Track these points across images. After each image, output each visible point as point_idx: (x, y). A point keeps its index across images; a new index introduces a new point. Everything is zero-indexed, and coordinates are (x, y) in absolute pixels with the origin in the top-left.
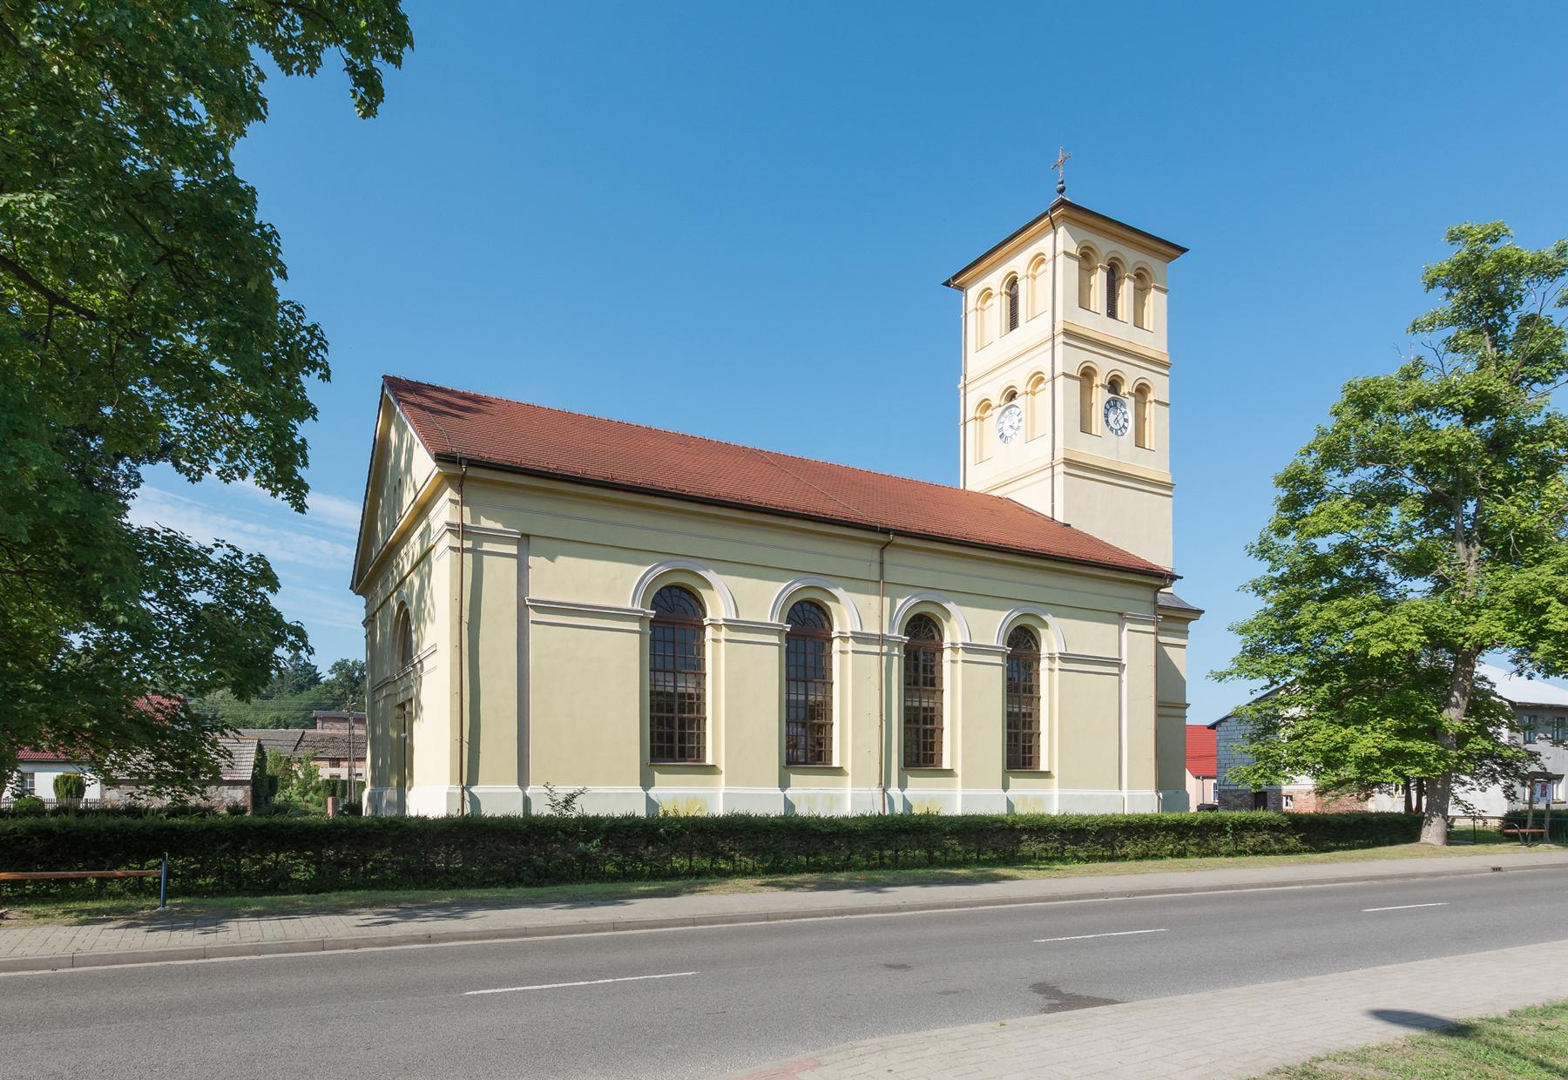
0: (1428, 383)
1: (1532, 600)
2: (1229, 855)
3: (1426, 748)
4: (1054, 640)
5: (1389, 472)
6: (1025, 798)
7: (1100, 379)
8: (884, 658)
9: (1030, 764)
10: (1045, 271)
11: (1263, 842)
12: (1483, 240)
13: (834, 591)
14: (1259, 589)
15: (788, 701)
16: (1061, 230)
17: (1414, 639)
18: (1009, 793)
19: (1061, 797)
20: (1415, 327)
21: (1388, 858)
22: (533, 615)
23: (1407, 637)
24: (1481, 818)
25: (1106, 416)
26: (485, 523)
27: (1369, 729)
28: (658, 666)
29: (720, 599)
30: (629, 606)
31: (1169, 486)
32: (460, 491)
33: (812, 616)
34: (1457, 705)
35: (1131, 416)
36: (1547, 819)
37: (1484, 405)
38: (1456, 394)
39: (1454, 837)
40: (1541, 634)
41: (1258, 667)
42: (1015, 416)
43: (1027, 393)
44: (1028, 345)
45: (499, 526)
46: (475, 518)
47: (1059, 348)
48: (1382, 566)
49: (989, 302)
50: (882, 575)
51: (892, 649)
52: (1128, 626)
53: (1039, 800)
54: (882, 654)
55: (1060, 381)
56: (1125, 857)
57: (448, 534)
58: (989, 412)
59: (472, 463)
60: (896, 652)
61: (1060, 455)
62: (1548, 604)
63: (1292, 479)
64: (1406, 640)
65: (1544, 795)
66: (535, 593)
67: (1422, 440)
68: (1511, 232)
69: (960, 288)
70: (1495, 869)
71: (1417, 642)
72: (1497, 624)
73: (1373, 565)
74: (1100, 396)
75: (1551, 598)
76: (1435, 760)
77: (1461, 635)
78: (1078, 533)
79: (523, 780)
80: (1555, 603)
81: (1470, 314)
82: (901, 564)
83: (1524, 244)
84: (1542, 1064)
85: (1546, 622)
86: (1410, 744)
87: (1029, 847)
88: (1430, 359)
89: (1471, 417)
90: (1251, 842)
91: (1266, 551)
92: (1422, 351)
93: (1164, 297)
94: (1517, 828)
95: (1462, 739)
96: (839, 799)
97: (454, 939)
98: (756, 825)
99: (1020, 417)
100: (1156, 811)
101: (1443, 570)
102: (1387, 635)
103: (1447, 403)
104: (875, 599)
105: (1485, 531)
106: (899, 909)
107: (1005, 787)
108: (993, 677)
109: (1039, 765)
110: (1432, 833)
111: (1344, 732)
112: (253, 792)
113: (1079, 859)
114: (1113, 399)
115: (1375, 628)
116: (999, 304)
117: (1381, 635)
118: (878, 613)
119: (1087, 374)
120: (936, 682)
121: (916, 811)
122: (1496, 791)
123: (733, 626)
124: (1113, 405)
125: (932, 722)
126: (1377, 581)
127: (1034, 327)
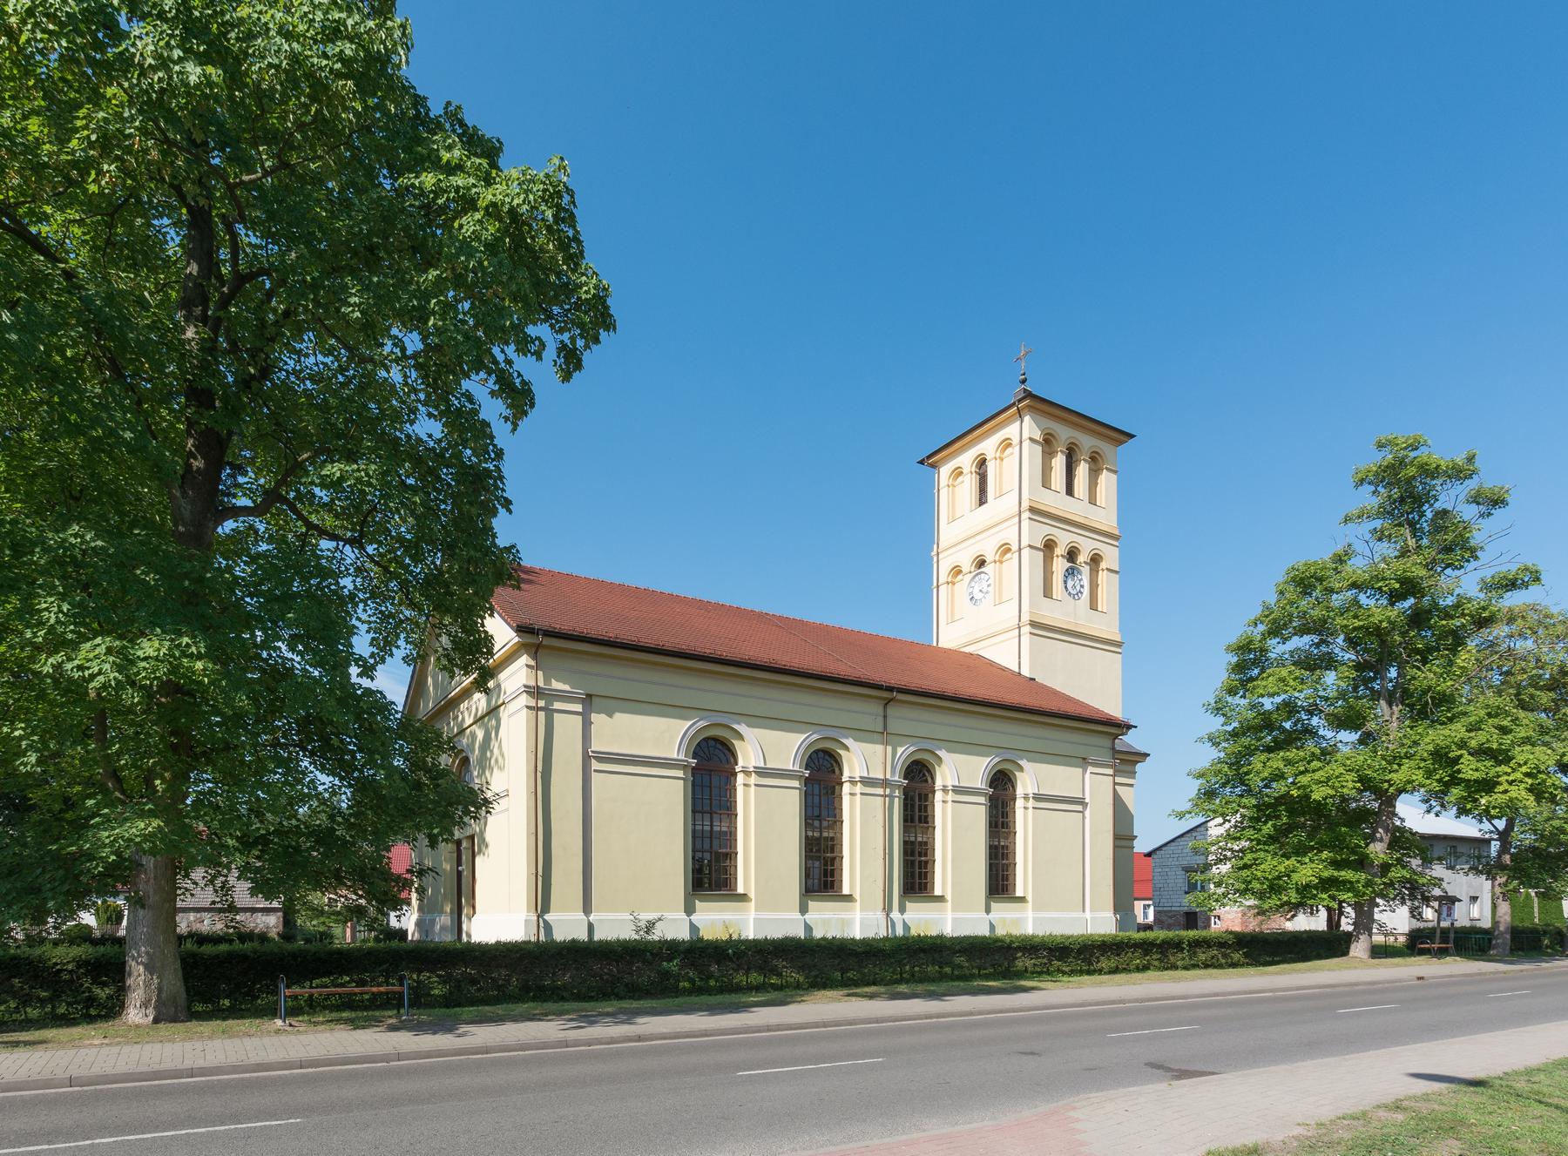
0: (1357, 567)
1: (1447, 753)
2: (1186, 968)
3: (1357, 876)
4: (1028, 782)
5: (1322, 642)
6: (1004, 920)
7: (1060, 550)
8: (887, 799)
9: (926, 889)
10: (1012, 454)
11: (1213, 958)
12: (1406, 448)
13: (845, 741)
14: (1214, 741)
15: (694, 831)
16: (1027, 419)
17: (1350, 786)
18: (991, 916)
19: (1035, 919)
20: (1347, 520)
21: (1329, 970)
22: (595, 765)
23: (1344, 784)
24: (1393, 934)
25: (1065, 582)
26: (557, 685)
27: (1307, 860)
28: (700, 808)
29: (750, 749)
30: (675, 756)
31: (1119, 644)
32: (535, 657)
34: (1381, 840)
35: (1086, 583)
36: (1452, 936)
37: (1409, 587)
38: (1384, 579)
39: (1379, 952)
40: (1454, 781)
41: (1212, 807)
43: (995, 562)
44: (996, 520)
45: (567, 688)
46: (547, 681)
47: (1025, 524)
48: (1315, 721)
49: (960, 479)
50: (885, 728)
51: (893, 791)
52: (1090, 769)
53: (1018, 921)
54: (886, 796)
55: (1026, 552)
56: (1100, 972)
57: (525, 694)
58: (960, 577)
60: (897, 794)
61: (1026, 618)
62: (1461, 756)
63: (1244, 647)
64: (1343, 787)
65: (1449, 915)
66: (596, 746)
67: (1356, 617)
68: (1429, 442)
69: (933, 466)
70: (1420, 978)
71: (1352, 789)
72: (1417, 772)
73: (1308, 719)
74: (1060, 565)
75: (1462, 752)
76: (1363, 886)
77: (1386, 781)
78: (1043, 687)
79: (587, 909)
80: (1466, 756)
81: (1393, 509)
82: (903, 718)
83: (1440, 452)
84: (1540, 1102)
85: (1459, 771)
86: (1343, 873)
87: (1023, 962)
88: (1359, 547)
89: (1395, 597)
90: (1202, 957)
91: (1221, 709)
92: (1352, 540)
93: (1114, 477)
94: (1418, 943)
95: (1385, 868)
96: (850, 923)
97: (657, 1039)
98: (804, 946)
100: (1114, 932)
101: (1371, 726)
102: (1325, 782)
103: (1376, 586)
104: (879, 748)
105: (1406, 693)
106: (971, 1014)
107: (988, 911)
108: (977, 815)
109: (1015, 891)
110: (1359, 949)
111: (1287, 863)
112: (284, 917)
113: (1064, 973)
114: (1071, 568)
115: (1317, 776)
116: (969, 483)
117: (1321, 782)
118: (882, 760)
119: (1049, 546)
120: (929, 819)
121: (914, 932)
122: (1403, 911)
123: (762, 772)
124: (1071, 572)
125: (926, 855)
126: (1310, 732)
127: (1003, 503)
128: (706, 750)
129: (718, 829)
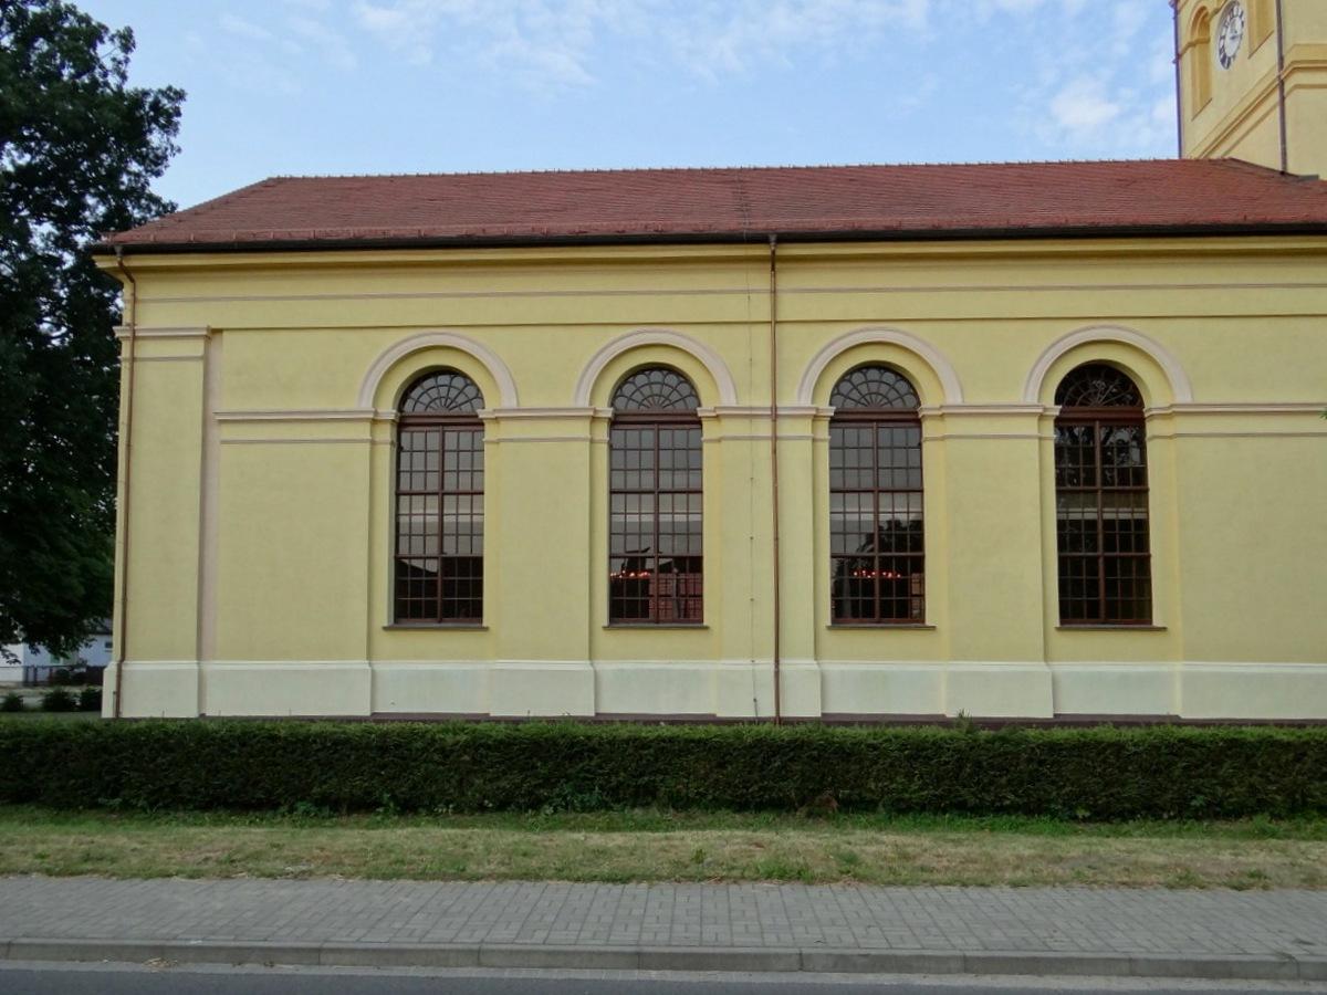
42: (1237, 18)
59: (786, 238)
129: (856, 517)
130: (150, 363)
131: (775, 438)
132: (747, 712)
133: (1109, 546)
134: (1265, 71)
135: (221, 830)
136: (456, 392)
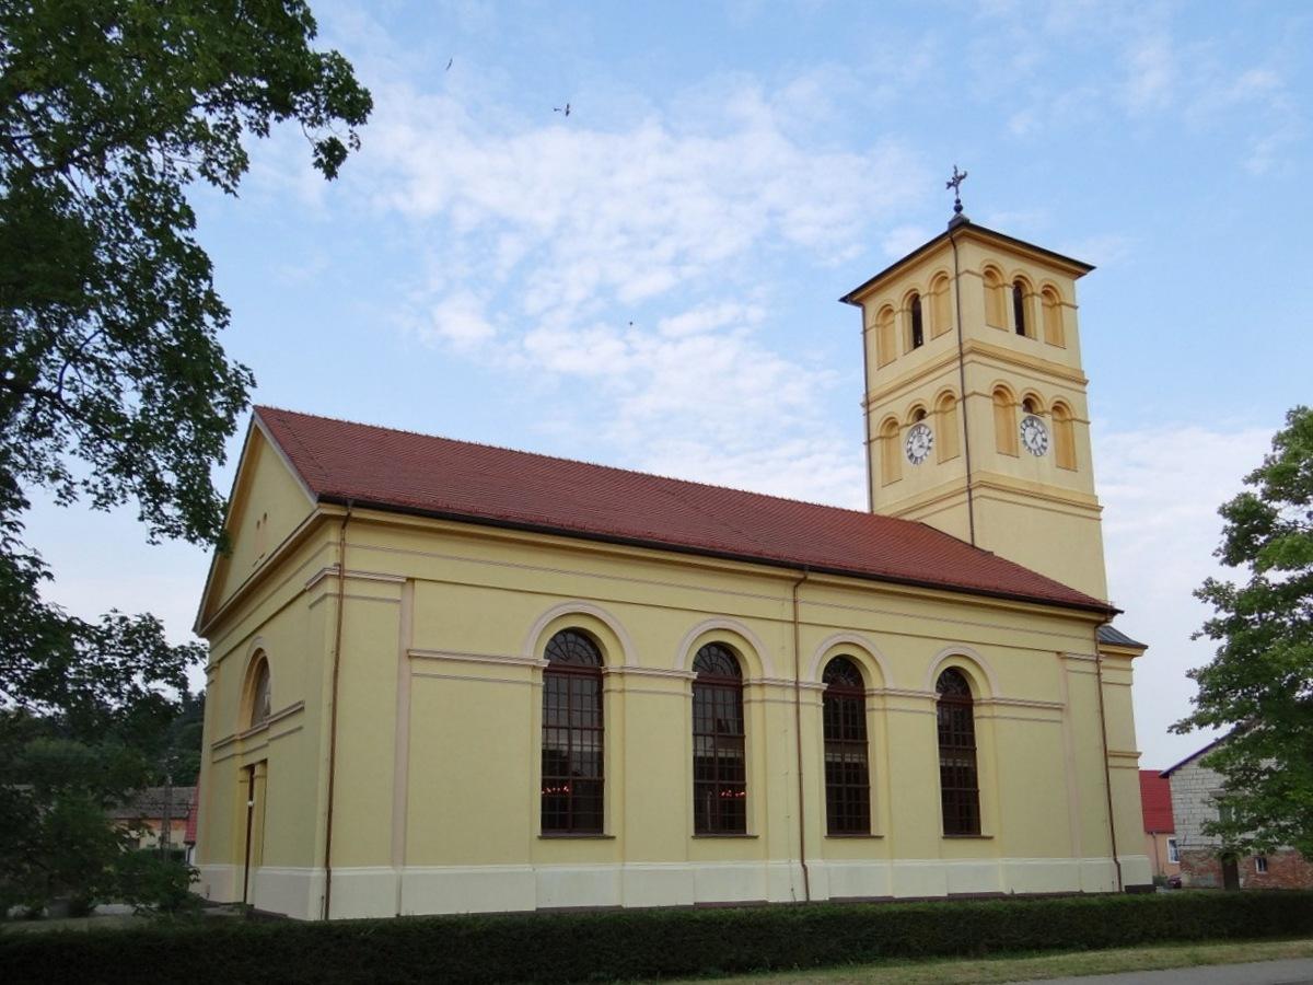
33: (578, 649)
49: (890, 318)
78: (1002, 561)
99: (930, 437)
128: (707, 659)
129: (579, 749)
130: (358, 602)
131: (797, 703)
132: (787, 899)
133: (848, 781)
134: (952, 478)
135: (1258, 949)
136: (557, 649)
